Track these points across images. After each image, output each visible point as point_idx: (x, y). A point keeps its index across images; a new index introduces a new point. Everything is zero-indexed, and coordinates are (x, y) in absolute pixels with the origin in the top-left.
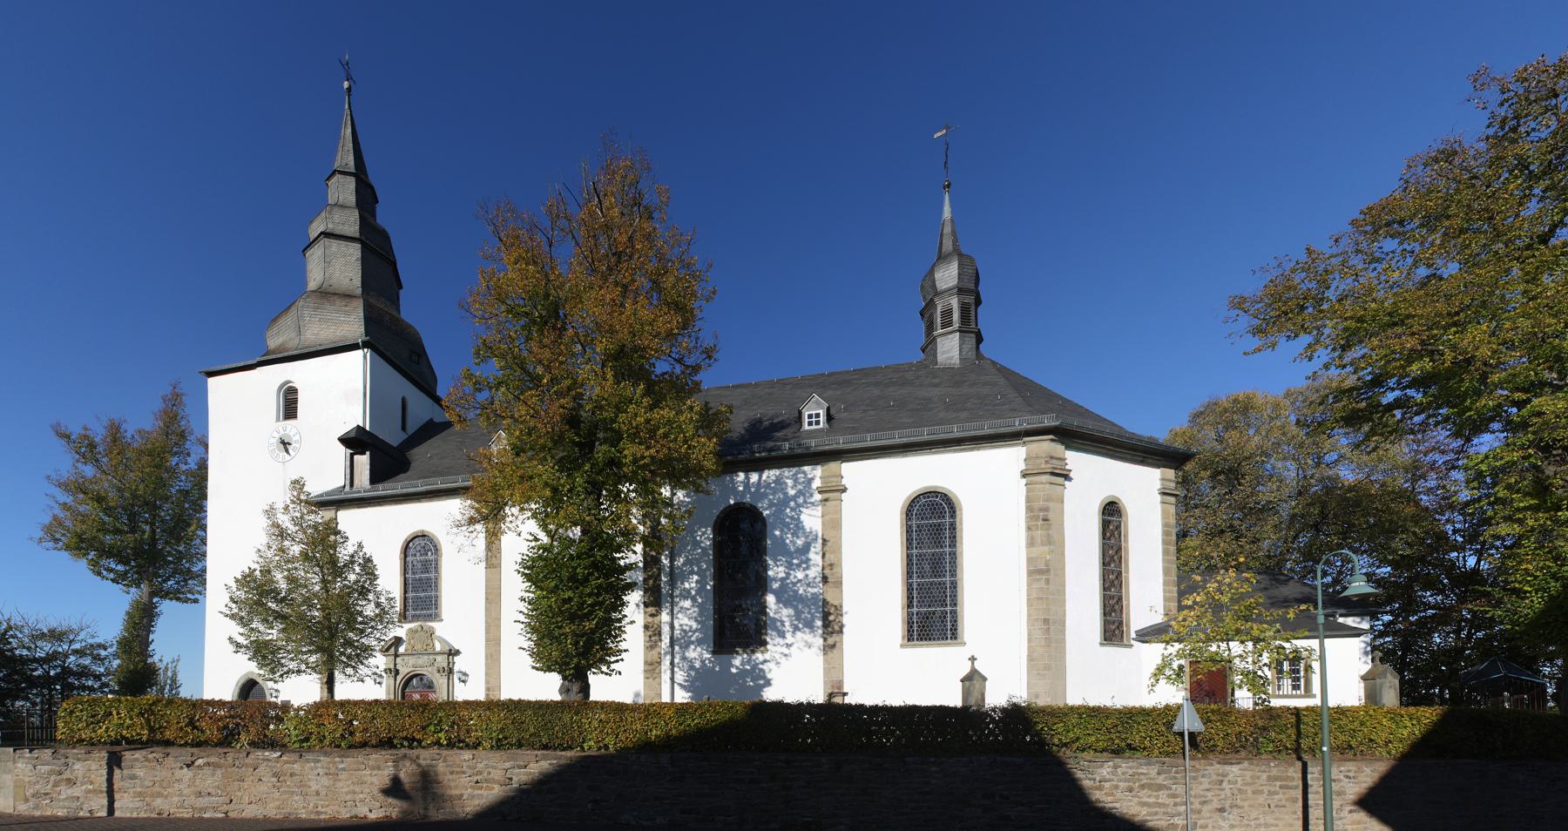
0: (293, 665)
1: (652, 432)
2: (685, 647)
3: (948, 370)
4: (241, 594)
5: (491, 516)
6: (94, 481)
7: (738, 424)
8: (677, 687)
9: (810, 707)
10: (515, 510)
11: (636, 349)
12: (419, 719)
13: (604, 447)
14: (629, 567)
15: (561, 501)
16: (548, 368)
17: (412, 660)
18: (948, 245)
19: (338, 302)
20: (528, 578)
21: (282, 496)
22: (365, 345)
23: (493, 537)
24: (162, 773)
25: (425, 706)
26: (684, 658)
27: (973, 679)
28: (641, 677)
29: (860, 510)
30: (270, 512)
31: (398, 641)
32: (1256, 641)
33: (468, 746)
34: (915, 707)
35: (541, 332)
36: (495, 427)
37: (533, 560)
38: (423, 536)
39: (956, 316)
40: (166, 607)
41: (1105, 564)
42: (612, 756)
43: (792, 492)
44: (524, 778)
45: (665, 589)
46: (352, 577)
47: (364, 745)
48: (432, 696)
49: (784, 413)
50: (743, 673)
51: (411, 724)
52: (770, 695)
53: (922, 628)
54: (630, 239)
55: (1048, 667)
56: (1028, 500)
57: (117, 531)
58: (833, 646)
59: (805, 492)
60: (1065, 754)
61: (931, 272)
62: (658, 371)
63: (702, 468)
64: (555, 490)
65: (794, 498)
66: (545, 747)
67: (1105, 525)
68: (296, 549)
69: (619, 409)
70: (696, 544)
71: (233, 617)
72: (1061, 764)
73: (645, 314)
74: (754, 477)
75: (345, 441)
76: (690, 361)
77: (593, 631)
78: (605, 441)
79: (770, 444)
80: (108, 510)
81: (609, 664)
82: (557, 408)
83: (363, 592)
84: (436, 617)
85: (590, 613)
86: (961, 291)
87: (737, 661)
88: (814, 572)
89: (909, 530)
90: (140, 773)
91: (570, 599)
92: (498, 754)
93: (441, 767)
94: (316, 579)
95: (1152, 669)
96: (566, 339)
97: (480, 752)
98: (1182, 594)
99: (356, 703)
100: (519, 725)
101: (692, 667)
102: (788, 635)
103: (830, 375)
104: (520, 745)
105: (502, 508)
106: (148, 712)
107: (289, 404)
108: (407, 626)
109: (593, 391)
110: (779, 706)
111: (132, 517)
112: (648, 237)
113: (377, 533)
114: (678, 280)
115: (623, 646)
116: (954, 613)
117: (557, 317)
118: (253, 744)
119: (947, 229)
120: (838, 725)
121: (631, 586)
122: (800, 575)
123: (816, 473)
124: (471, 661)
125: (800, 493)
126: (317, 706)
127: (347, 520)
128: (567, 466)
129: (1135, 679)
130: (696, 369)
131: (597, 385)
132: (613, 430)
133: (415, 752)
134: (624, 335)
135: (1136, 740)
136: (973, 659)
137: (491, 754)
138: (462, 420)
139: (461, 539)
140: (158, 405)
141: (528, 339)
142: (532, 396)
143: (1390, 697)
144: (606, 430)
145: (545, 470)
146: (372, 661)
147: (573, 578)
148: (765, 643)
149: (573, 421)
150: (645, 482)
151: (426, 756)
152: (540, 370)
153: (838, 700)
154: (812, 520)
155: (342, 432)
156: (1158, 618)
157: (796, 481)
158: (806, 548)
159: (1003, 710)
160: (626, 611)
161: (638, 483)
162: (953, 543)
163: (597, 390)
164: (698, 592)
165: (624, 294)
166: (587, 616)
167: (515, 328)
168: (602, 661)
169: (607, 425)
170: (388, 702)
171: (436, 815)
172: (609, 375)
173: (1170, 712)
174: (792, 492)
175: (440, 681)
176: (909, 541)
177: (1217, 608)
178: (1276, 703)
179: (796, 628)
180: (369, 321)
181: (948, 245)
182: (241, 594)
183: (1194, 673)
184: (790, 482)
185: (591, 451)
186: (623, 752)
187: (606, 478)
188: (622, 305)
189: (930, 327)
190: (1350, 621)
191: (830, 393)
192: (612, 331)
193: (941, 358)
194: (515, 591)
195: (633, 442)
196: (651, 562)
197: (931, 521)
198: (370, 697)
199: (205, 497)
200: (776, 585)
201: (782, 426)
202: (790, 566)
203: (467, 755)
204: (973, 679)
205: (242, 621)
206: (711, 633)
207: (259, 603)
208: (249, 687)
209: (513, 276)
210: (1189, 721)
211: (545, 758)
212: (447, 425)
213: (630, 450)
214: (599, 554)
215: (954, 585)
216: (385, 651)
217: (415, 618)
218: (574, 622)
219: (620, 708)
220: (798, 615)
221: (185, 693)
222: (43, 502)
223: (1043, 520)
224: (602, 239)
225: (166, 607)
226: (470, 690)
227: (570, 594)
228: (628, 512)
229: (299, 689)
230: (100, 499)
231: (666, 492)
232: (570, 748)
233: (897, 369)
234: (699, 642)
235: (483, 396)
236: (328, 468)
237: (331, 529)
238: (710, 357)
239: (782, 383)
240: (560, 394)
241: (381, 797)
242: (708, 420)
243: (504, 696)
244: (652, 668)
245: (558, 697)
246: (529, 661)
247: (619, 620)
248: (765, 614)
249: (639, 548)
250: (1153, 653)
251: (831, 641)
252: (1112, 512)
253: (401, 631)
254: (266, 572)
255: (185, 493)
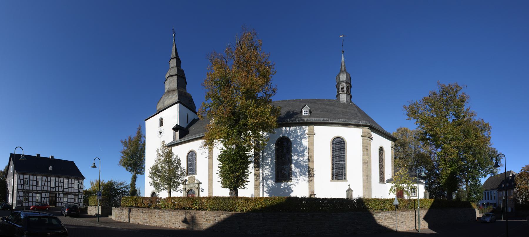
0: (162, 188)
1: (257, 115)
2: (267, 180)
3: (343, 104)
4: (152, 171)
5: (210, 144)
6: (127, 150)
7: (283, 113)
8: (264, 193)
9: (305, 199)
10: (217, 141)
11: (252, 90)
12: (191, 202)
13: (242, 120)
14: (250, 156)
15: (230, 137)
16: (226, 98)
17: (189, 186)
18: (343, 69)
19: (172, 93)
20: (220, 161)
21: (160, 146)
22: (178, 102)
23: (211, 149)
24: (137, 214)
25: (193, 198)
26: (266, 184)
27: (349, 191)
28: (253, 189)
29: (319, 141)
30: (157, 150)
31: (186, 181)
32: (408, 184)
33: (204, 210)
34: (334, 199)
35: (224, 88)
36: (211, 118)
37: (222, 155)
38: (192, 151)
39: (345, 89)
40: (138, 176)
41: (380, 163)
42: (245, 213)
43: (299, 134)
44: (219, 219)
45: (261, 163)
46: (175, 164)
47: (178, 209)
48: (194, 196)
49: (297, 110)
50: (284, 188)
51: (189, 203)
52: (293, 195)
53: (336, 176)
54: (250, 57)
55: (367, 188)
56: (363, 143)
57: (130, 160)
58: (311, 180)
59: (303, 134)
60: (371, 211)
61: (339, 75)
62: (259, 96)
63: (272, 126)
64: (228, 134)
65: (300, 136)
66: (225, 210)
67: (380, 153)
68: (163, 159)
69: (247, 109)
70: (270, 149)
71: (150, 177)
72: (370, 213)
73: (255, 79)
74: (288, 129)
75: (174, 129)
76: (268, 93)
77: (239, 176)
78: (243, 118)
79: (293, 119)
80: (129, 156)
81: (244, 185)
82: (228, 110)
83: (178, 168)
84: (195, 173)
85: (238, 170)
86: (346, 82)
87: (283, 185)
88: (306, 158)
89: (333, 148)
90: (134, 213)
91: (232, 166)
92: (212, 212)
93: (197, 215)
94: (167, 166)
95: (389, 190)
96: (231, 89)
97: (207, 211)
98: (395, 172)
99: (176, 198)
100: (218, 204)
101: (269, 186)
102: (298, 177)
103: (311, 100)
104: (218, 210)
105: (213, 141)
106: (135, 200)
107: (161, 123)
108: (188, 176)
109: (239, 104)
110: (296, 198)
111: (133, 157)
112: (256, 56)
113: (181, 152)
114: (265, 68)
115: (248, 180)
116: (345, 172)
117: (229, 83)
118: (154, 208)
119: (343, 64)
120: (313, 203)
121: (250, 162)
122: (302, 159)
123: (306, 129)
124: (205, 186)
125: (302, 134)
126: (167, 198)
127: (174, 149)
128: (232, 127)
129: (384, 192)
130: (270, 95)
131: (240, 101)
132: (245, 115)
133: (191, 211)
134: (248, 86)
135: (386, 207)
136: (349, 185)
137: (210, 212)
138: (202, 117)
139: (202, 151)
140: (136, 130)
141: (220, 90)
142: (221, 108)
143: (428, 197)
144: (243, 115)
145: (225, 129)
146: (180, 186)
147: (233, 160)
148: (291, 179)
149: (233, 113)
150: (255, 130)
151: (193, 212)
152: (224, 99)
153: (313, 196)
154: (305, 142)
155: (173, 127)
156: (391, 177)
157: (300, 130)
158: (303, 151)
159: (357, 199)
160: (249, 169)
161: (252, 130)
162: (344, 153)
163: (240, 103)
164: (271, 163)
165: (248, 74)
166: (237, 171)
167: (216, 88)
168: (242, 185)
169: (243, 113)
170: (184, 197)
171: (196, 229)
172: (244, 98)
173: (393, 200)
174: (299, 134)
175: (196, 191)
176: (333, 151)
177: (401, 176)
178: (411, 198)
179: (300, 175)
180: (179, 95)
181: (343, 69)
182: (152, 171)
183: (397, 191)
184: (299, 131)
185: (239, 121)
186: (248, 212)
187: (242, 130)
188: (248, 77)
189: (338, 91)
190: (422, 181)
191: (310, 105)
192: (245, 85)
193: (341, 100)
194: (217, 164)
195: (251, 118)
196: (256, 154)
197: (339, 146)
198: (179, 196)
199: (145, 149)
200: (294, 162)
201: (296, 114)
202: (299, 156)
203: (204, 212)
204: (349, 191)
205: (152, 178)
206: (275, 176)
207: (155, 173)
208: (153, 194)
209: (216, 73)
210: (396, 202)
211: (225, 214)
212: (199, 119)
213: (250, 121)
214: (241, 152)
215: (345, 164)
216: (183, 183)
217: (190, 174)
218: (234, 175)
219: (247, 199)
220: (301, 171)
221: (141, 196)
222: (118, 157)
223: (366, 149)
224: (242, 58)
225: (138, 176)
226: (204, 194)
227: (232, 165)
228: (250, 139)
229: (163, 194)
230: (127, 154)
231: (261, 133)
232: (232, 211)
233: (329, 101)
234: (271, 179)
235: (208, 110)
236: (169, 136)
237: (170, 152)
238: (274, 92)
239: (296, 101)
240: (229, 106)
241: (182, 223)
242: (274, 111)
243: (214, 195)
244: (257, 187)
245: (229, 196)
246: (221, 185)
247: (247, 172)
248: (291, 170)
249: (253, 150)
250: (389, 186)
251: (311, 179)
252: (381, 149)
253: (186, 178)
254: (157, 165)
255: (141, 149)
